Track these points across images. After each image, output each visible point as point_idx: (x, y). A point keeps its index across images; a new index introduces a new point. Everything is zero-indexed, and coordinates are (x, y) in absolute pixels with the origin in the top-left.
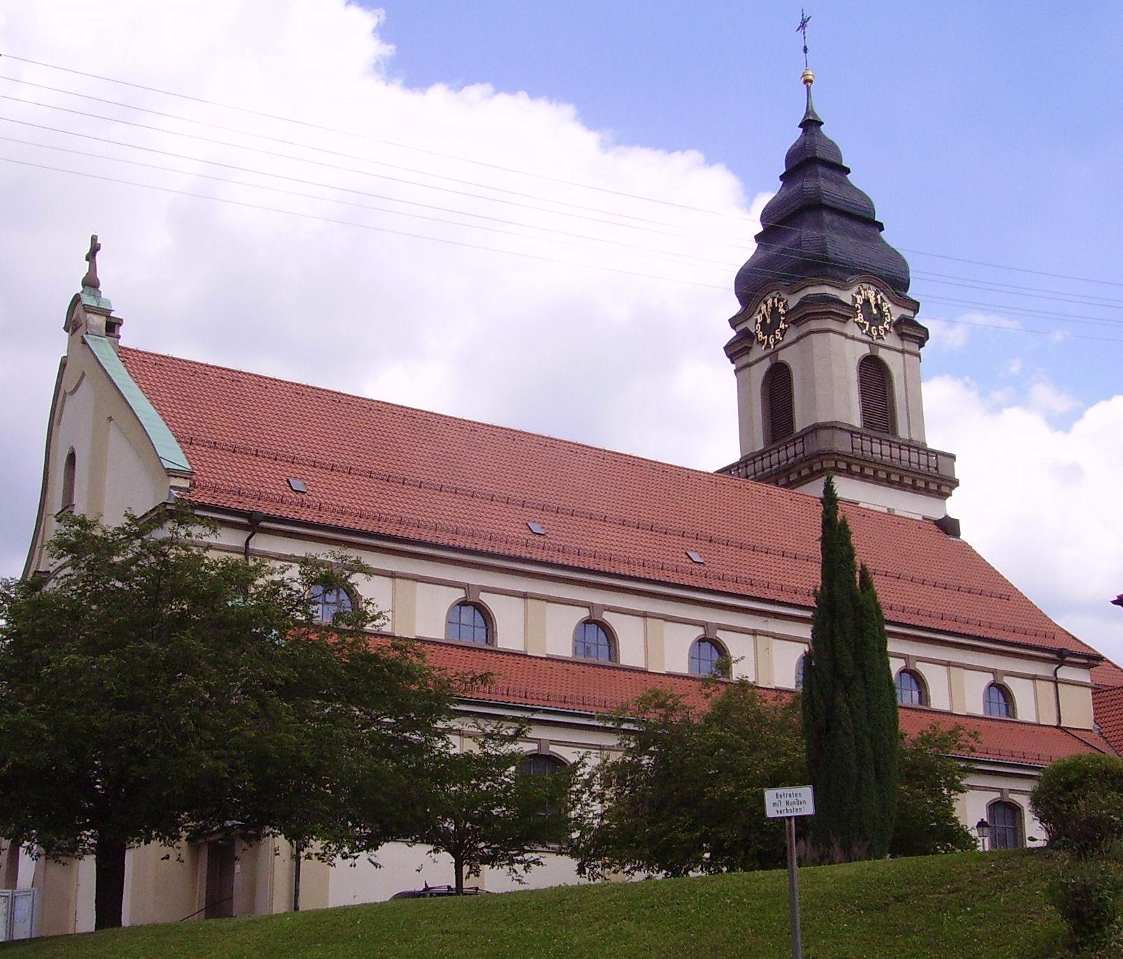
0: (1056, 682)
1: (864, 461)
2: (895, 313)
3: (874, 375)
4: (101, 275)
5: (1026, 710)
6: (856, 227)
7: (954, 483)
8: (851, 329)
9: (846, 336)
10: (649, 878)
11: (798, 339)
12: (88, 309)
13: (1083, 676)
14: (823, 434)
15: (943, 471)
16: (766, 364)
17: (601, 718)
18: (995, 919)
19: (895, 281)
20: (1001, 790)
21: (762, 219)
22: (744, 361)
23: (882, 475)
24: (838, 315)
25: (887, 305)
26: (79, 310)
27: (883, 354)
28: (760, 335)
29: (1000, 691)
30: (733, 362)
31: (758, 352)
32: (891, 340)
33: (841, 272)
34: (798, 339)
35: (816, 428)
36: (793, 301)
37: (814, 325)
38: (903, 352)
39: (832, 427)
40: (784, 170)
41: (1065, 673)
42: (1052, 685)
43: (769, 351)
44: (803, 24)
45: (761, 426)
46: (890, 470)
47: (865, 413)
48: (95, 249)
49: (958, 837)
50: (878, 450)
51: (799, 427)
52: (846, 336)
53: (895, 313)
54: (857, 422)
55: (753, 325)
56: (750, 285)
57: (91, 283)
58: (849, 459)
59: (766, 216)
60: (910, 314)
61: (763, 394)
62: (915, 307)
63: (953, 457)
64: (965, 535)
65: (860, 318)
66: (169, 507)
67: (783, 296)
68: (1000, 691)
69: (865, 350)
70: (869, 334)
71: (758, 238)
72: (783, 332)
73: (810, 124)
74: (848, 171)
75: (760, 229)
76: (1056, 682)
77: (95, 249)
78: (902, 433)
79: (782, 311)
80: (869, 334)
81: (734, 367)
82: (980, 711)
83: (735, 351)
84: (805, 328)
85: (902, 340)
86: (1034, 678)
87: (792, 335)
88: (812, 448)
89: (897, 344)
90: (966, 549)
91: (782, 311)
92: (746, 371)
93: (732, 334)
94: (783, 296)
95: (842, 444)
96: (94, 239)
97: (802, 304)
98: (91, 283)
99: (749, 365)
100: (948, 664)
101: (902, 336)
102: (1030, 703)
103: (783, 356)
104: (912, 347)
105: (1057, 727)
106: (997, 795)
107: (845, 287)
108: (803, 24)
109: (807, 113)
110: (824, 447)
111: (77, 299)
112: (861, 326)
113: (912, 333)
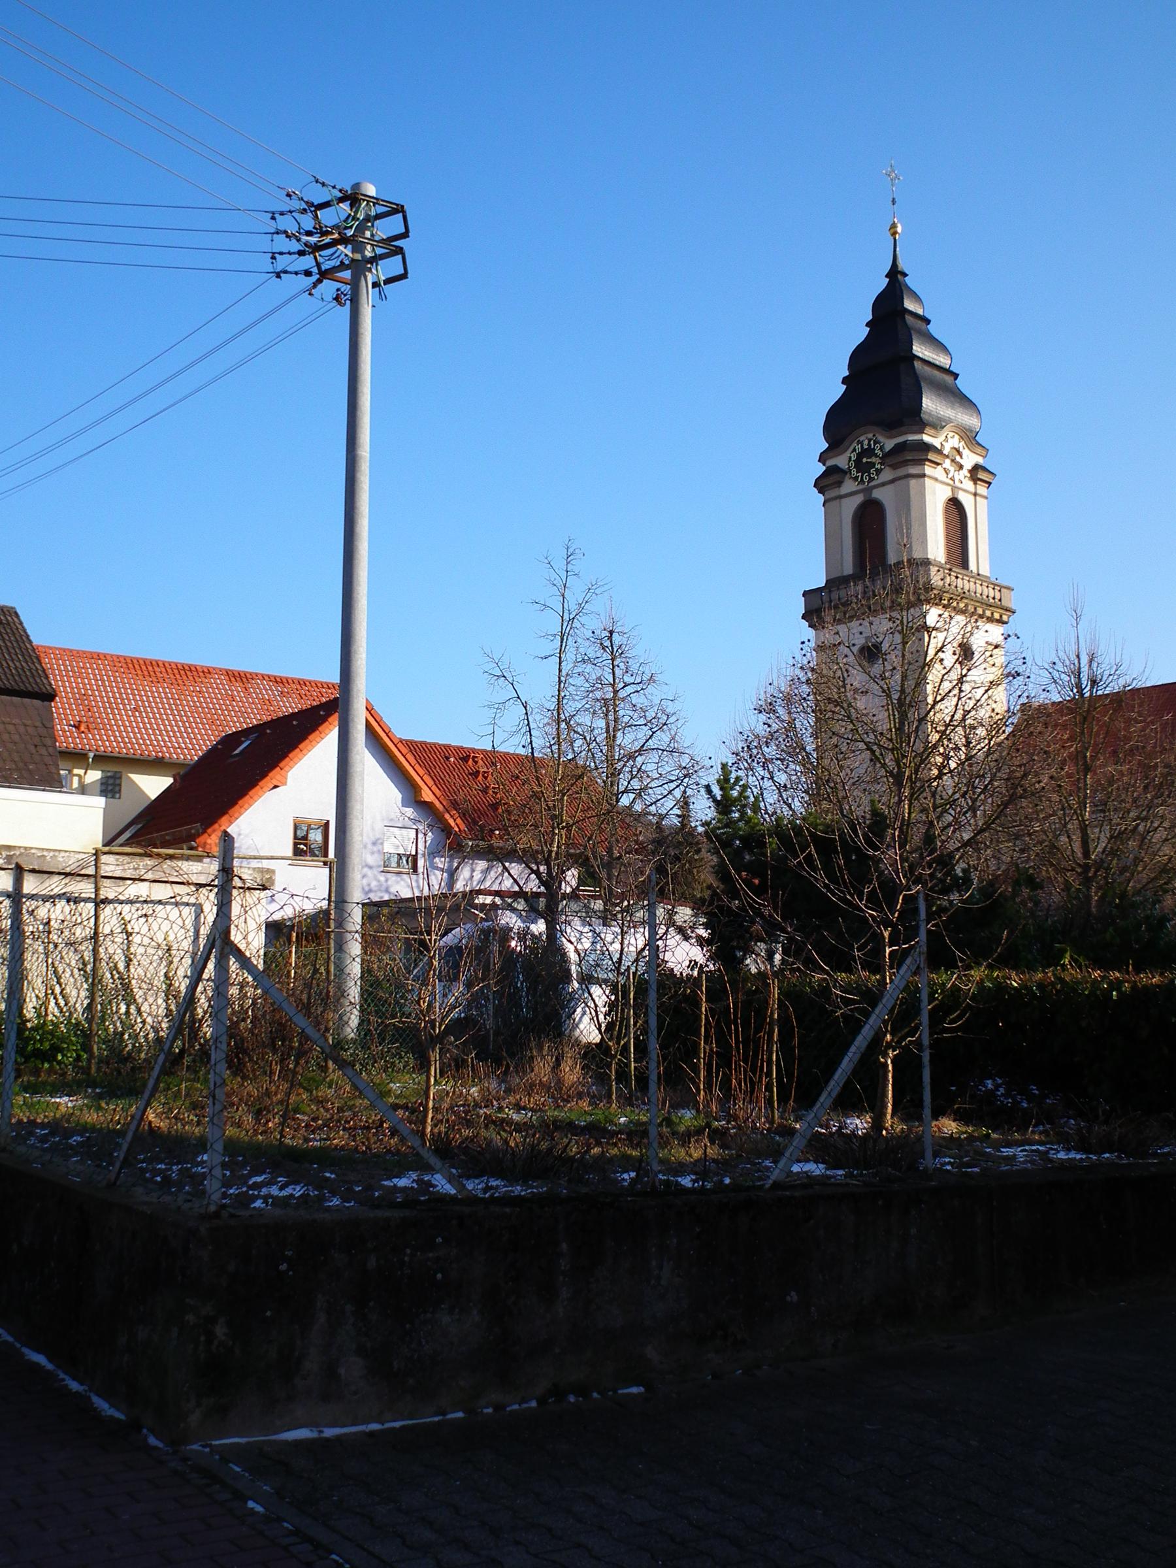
0: (975, 494)
9: (936, 479)
10: (321, 1432)
16: (859, 499)
18: (1026, 818)
22: (832, 493)
28: (854, 472)
31: (849, 486)
36: (889, 444)
40: (870, 317)
43: (861, 487)
45: (850, 542)
49: (936, 1115)
53: (970, 459)
56: (840, 424)
66: (481, 900)
67: (881, 438)
72: (878, 472)
75: (847, 373)
78: (972, 566)
80: (953, 479)
81: (821, 498)
83: (821, 485)
84: (901, 472)
85: (975, 484)
92: (835, 503)
94: (881, 438)
99: (841, 497)
103: (877, 494)
112: (946, 471)
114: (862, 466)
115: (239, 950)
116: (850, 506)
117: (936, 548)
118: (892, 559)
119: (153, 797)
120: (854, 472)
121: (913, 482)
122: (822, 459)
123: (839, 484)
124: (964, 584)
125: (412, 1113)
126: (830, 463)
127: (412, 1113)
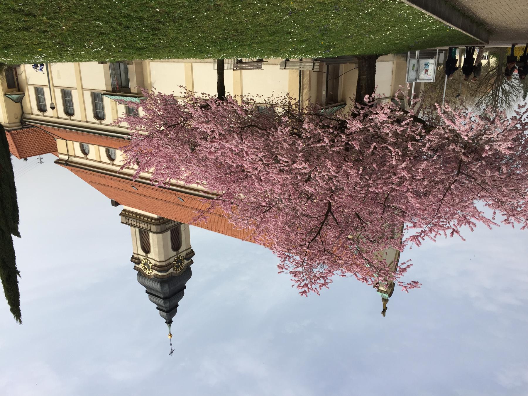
0: (68, 155)
1: (146, 222)
2: (141, 266)
3: (146, 249)
4: (382, 303)
5: (77, 145)
6: (153, 292)
7: (121, 214)
8: (153, 262)
9: (154, 260)
11: (169, 259)
12: (386, 292)
13: (61, 156)
14: (158, 231)
15: (124, 218)
16: (180, 251)
17: (122, 138)
19: (141, 274)
20: (101, 124)
21: (183, 293)
22: (189, 250)
23: (142, 218)
25: (143, 269)
26: (389, 292)
27: (144, 254)
28: (182, 259)
29: (85, 152)
30: (192, 250)
31: (184, 254)
32: (142, 258)
33: (156, 279)
34: (169, 259)
35: (162, 232)
36: (171, 270)
37: (164, 264)
38: (138, 254)
39: (157, 233)
41: (66, 158)
42: (70, 154)
44: (172, 352)
48: (384, 312)
50: (143, 226)
51: (169, 231)
52: (154, 260)
53: (141, 266)
54: (151, 235)
55: (186, 262)
56: (187, 273)
57: (385, 301)
58: (151, 223)
59: (183, 294)
60: (137, 266)
61: (181, 241)
62: (135, 268)
63: (121, 222)
64: (109, 201)
65: (150, 265)
68: (85, 152)
69: (149, 255)
70: (148, 260)
72: (175, 261)
73: (169, 322)
74: (157, 308)
76: (68, 155)
77: (384, 312)
78: (137, 230)
79: (175, 267)
80: (148, 260)
82: (90, 146)
83: (192, 253)
84: (167, 262)
86: (75, 156)
87: (172, 260)
88: (163, 226)
89: (140, 256)
90: (109, 196)
91: (175, 267)
94: (175, 272)
95: (153, 228)
96: (384, 315)
97: (168, 270)
98: (385, 301)
99: (186, 250)
100: (101, 162)
101: (138, 259)
102: (75, 148)
104: (135, 256)
105: (67, 140)
106: (103, 122)
107: (155, 275)
108: (172, 352)
109: (170, 326)
110: (159, 227)
111: (390, 295)
112: (150, 263)
113: (135, 260)
114: (180, 261)
115: (339, 58)
116: (183, 248)
117: (153, 238)
118: (168, 233)
119: (377, 64)
120: (182, 259)
121: (163, 259)
122: (192, 262)
123: (187, 254)
124: (143, 226)
125: (335, 261)
126: (190, 260)
127: (335, 261)
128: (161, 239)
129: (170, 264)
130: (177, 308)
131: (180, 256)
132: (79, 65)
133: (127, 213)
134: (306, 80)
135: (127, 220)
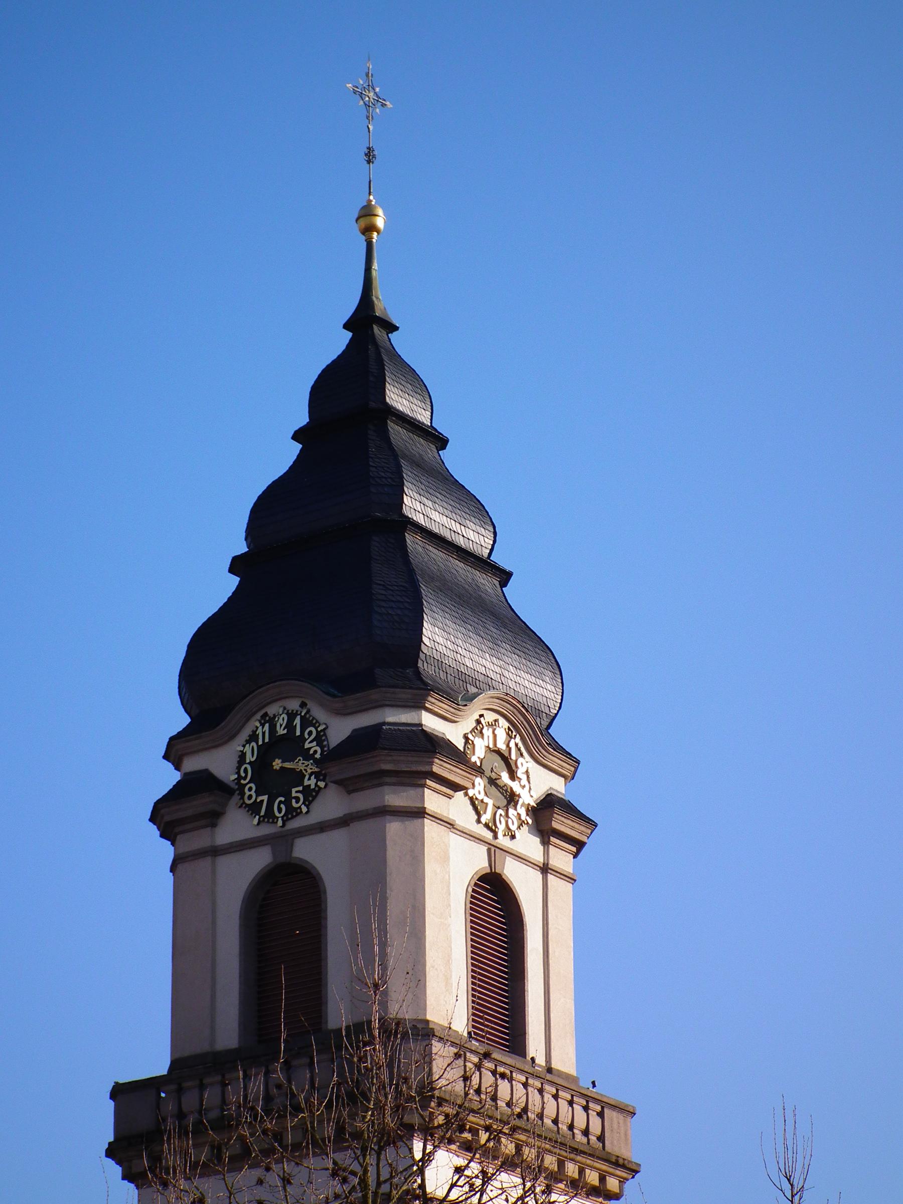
9: (450, 825)
11: (345, 821)
16: (260, 860)
24: (396, 773)
25: (525, 764)
28: (250, 790)
31: (236, 825)
32: (528, 843)
34: (345, 821)
36: (339, 730)
43: (267, 830)
46: (590, 1099)
47: (478, 1012)
53: (536, 781)
54: (461, 1024)
55: (221, 762)
67: (318, 713)
70: (491, 828)
71: (237, 565)
72: (310, 795)
80: (491, 828)
84: (365, 801)
93: (168, 777)
94: (318, 713)
99: (215, 852)
103: (306, 850)
116: (238, 875)
121: (394, 828)
122: (174, 751)
123: (213, 818)
126: (193, 764)
128: (396, 988)
129: (350, 786)
130: (303, 419)
131: (270, 816)
132: (490, 554)
133: (592, 1178)
134: (416, 759)
135: (595, 1126)
